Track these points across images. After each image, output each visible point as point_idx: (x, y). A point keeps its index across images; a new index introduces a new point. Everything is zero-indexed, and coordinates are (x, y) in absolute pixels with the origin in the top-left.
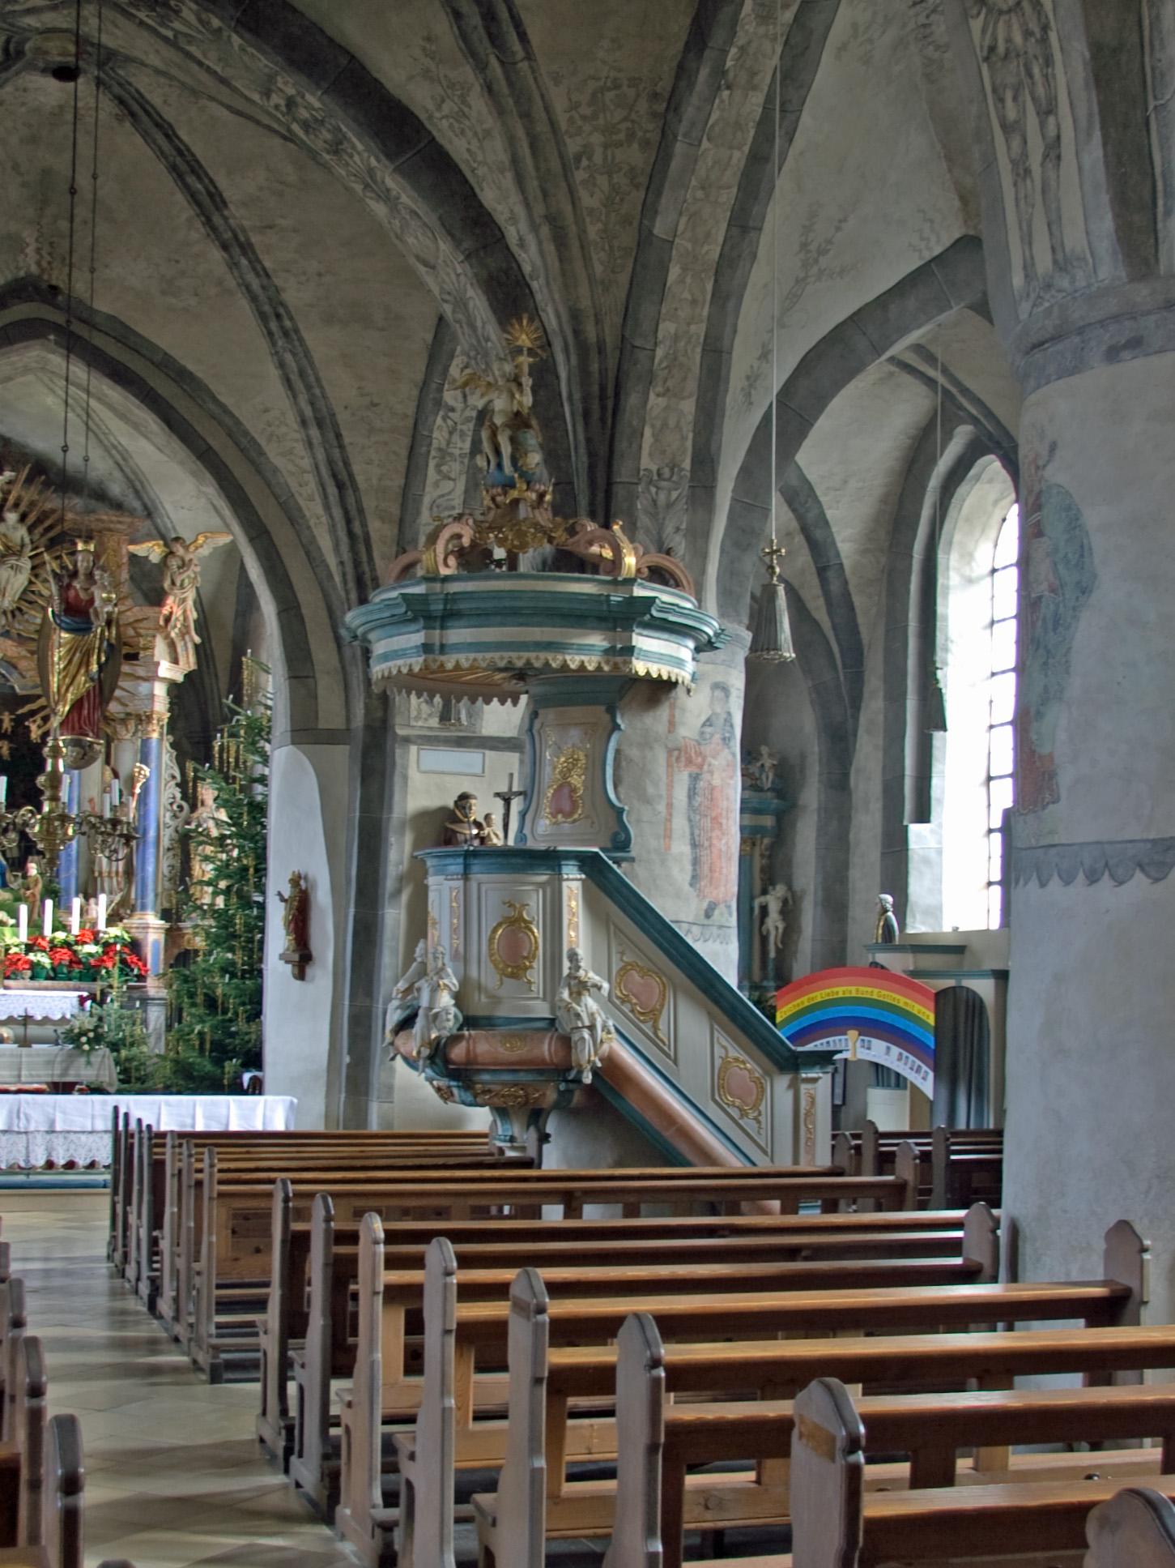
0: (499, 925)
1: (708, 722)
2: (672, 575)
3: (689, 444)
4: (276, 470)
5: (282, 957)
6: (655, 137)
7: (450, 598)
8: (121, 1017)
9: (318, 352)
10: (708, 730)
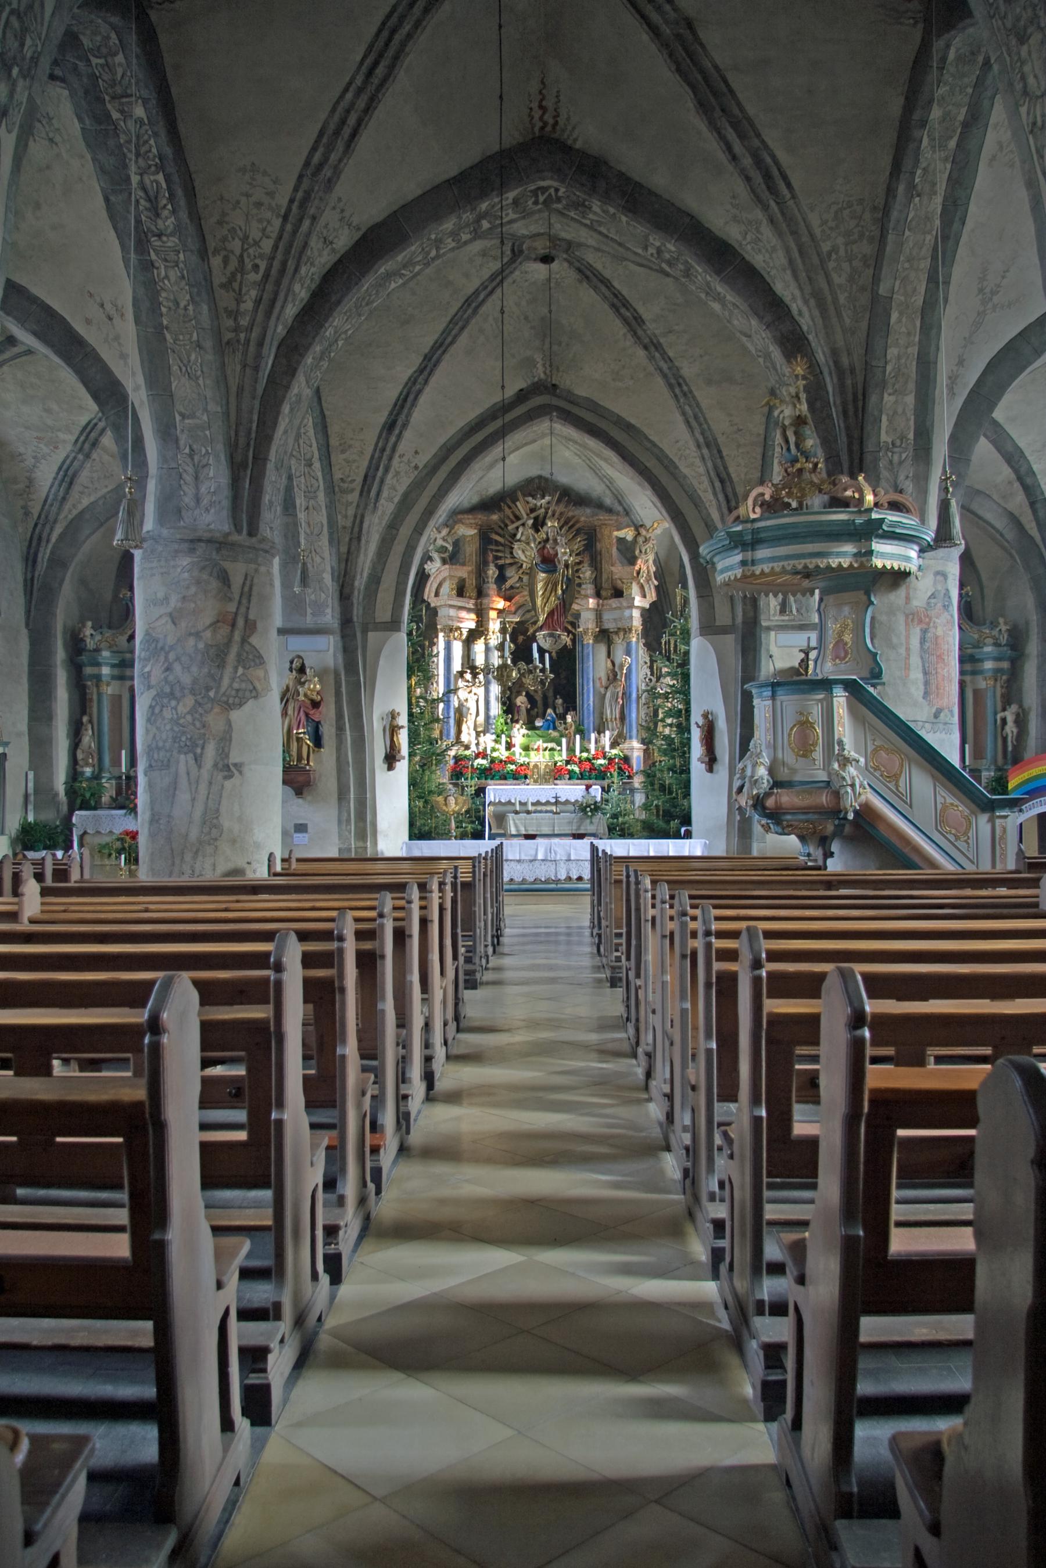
0: (795, 726)
1: (933, 596)
2: (904, 506)
3: (912, 423)
4: (685, 477)
5: (699, 760)
6: (878, 233)
7: (756, 532)
8: (619, 800)
9: (704, 403)
10: (933, 601)
